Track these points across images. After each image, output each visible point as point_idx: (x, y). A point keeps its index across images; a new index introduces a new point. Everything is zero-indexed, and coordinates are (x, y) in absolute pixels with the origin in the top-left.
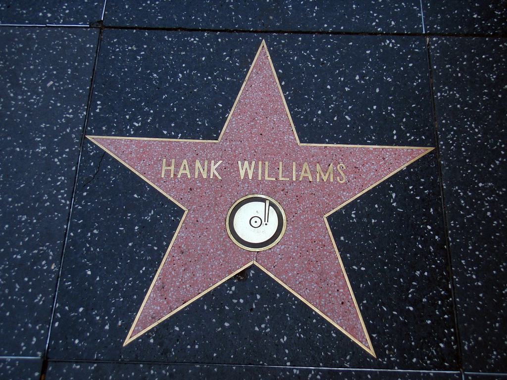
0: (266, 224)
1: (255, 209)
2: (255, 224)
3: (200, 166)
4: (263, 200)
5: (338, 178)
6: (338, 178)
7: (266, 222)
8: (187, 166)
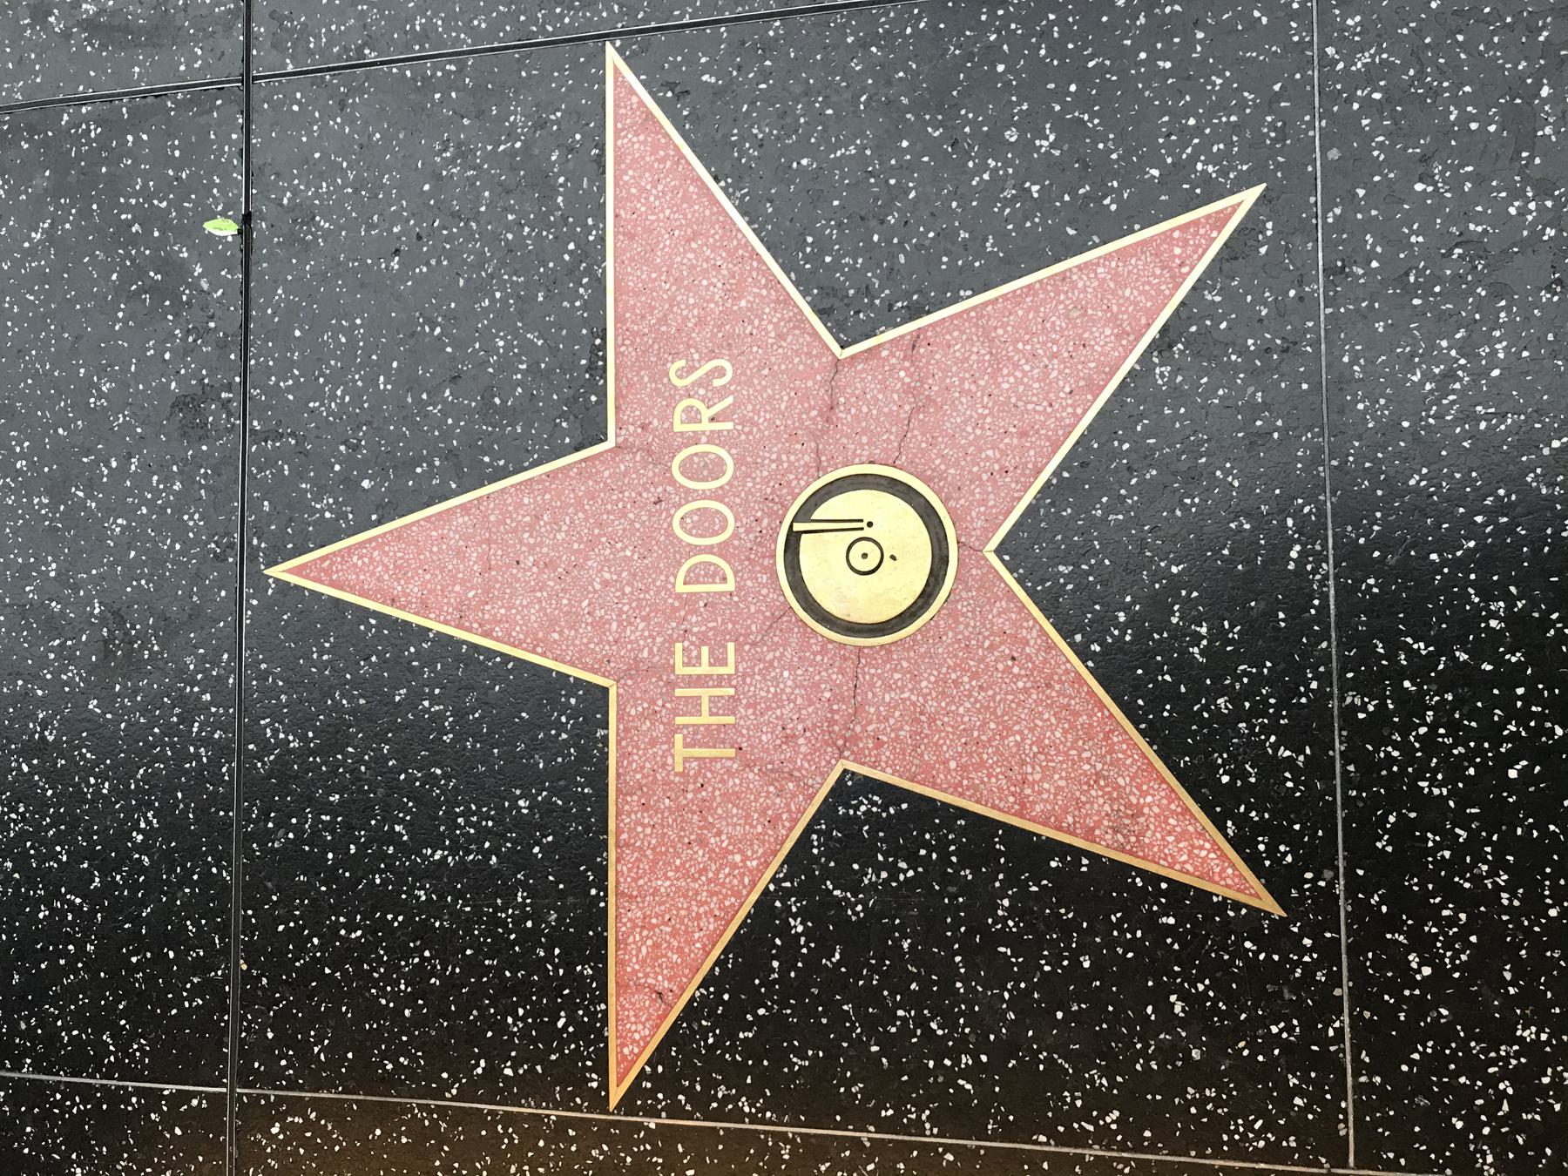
1: (822, 562)
2: (870, 561)
4: (793, 540)
5: (717, 383)
6: (717, 383)
7: (863, 525)
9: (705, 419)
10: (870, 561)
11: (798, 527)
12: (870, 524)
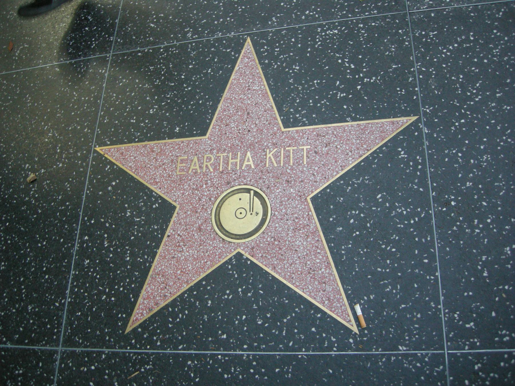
0: (251, 214)
2: (239, 215)
4: (248, 191)
8: (250, 159)
9: (207, 163)
11: (252, 192)
12: (251, 214)
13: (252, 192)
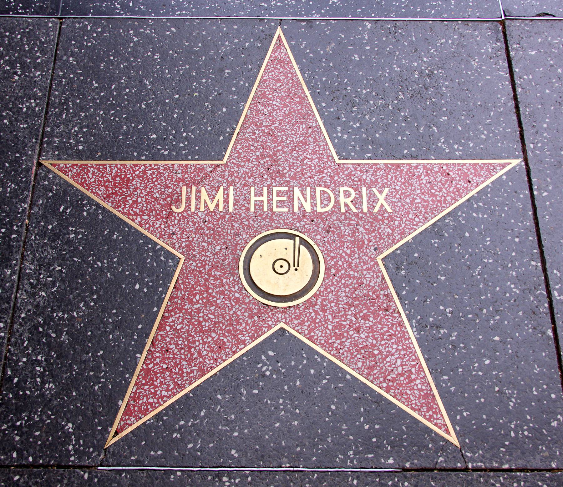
0: (296, 270)
3: (113, 430)
4: (292, 237)
10: (277, 269)
11: (297, 239)
13: (297, 239)
